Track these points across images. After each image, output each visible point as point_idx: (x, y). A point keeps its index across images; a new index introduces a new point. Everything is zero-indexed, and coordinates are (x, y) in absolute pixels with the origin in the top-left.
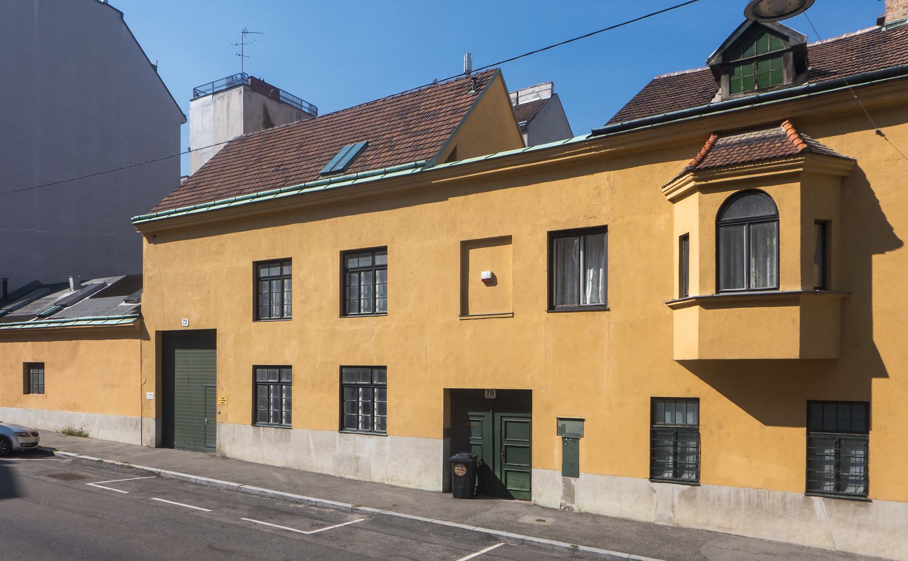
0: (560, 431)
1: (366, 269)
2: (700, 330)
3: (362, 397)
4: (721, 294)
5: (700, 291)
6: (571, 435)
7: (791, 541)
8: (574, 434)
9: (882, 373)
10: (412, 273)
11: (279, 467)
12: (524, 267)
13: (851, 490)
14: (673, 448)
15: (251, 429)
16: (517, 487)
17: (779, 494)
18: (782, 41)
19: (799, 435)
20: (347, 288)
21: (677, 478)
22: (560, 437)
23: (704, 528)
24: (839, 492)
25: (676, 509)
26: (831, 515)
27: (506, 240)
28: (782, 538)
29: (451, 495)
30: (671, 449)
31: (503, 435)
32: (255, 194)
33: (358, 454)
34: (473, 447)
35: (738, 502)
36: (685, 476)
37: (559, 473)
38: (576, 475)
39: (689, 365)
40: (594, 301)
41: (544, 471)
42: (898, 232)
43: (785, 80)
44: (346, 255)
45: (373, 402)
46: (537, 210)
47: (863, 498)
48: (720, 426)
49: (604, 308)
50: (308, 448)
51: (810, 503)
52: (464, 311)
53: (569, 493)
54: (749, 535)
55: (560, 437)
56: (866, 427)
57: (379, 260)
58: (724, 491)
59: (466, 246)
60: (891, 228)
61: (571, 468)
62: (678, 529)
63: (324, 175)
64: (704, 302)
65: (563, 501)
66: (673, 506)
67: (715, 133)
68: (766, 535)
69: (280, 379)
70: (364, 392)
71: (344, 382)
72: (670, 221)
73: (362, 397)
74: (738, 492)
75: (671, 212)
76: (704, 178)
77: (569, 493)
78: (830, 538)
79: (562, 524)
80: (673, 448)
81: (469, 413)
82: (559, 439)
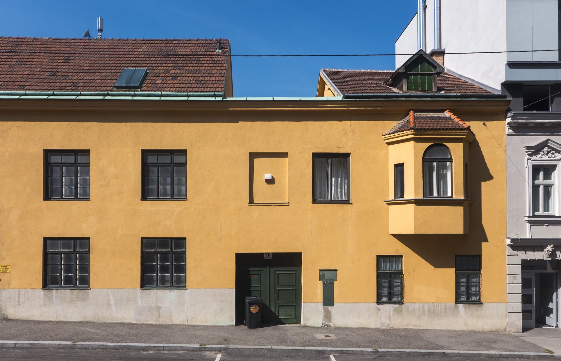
0: (321, 278)
1: (68, 165)
2: (415, 218)
3: (163, 262)
4: (425, 198)
5: (415, 196)
6: (328, 279)
7: (449, 328)
8: (330, 279)
9: (486, 240)
10: (209, 171)
11: (75, 322)
12: (295, 174)
13: (473, 299)
14: (389, 284)
15: (42, 292)
16: (286, 316)
17: (443, 305)
18: (432, 68)
19: (451, 272)
20: (49, 178)
21: (390, 301)
22: (321, 282)
23: (407, 327)
24: (468, 302)
25: (392, 319)
26: (466, 313)
27: (283, 155)
28: (444, 328)
29: (243, 327)
30: (387, 285)
31: (276, 282)
32: (51, 92)
33: (159, 305)
34: (252, 292)
35: (424, 311)
36: (395, 299)
37: (321, 304)
38: (332, 304)
39: (400, 237)
40: (336, 197)
41: (310, 304)
42: (492, 172)
43: (434, 88)
44: (145, 153)
45: (61, 264)
46: (308, 138)
47: (479, 303)
48: (414, 270)
49: (348, 202)
50: (109, 304)
51: (458, 308)
52: (251, 201)
53: (328, 316)
54: (429, 328)
55: (321, 282)
56: (479, 267)
57: (178, 159)
58: (417, 306)
59: (253, 156)
60: (489, 170)
61: (328, 300)
62: (393, 329)
63: (118, 87)
64: (417, 202)
65: (324, 322)
66: (390, 317)
67: (413, 110)
68: (438, 327)
69: (75, 249)
70: (65, 257)
71: (144, 250)
72: (387, 155)
73: (163, 262)
74: (423, 306)
75: (387, 150)
76: (419, 134)
77: (328, 316)
78: (466, 324)
79: (342, 336)
80: (389, 284)
81: (251, 269)
82: (320, 284)
